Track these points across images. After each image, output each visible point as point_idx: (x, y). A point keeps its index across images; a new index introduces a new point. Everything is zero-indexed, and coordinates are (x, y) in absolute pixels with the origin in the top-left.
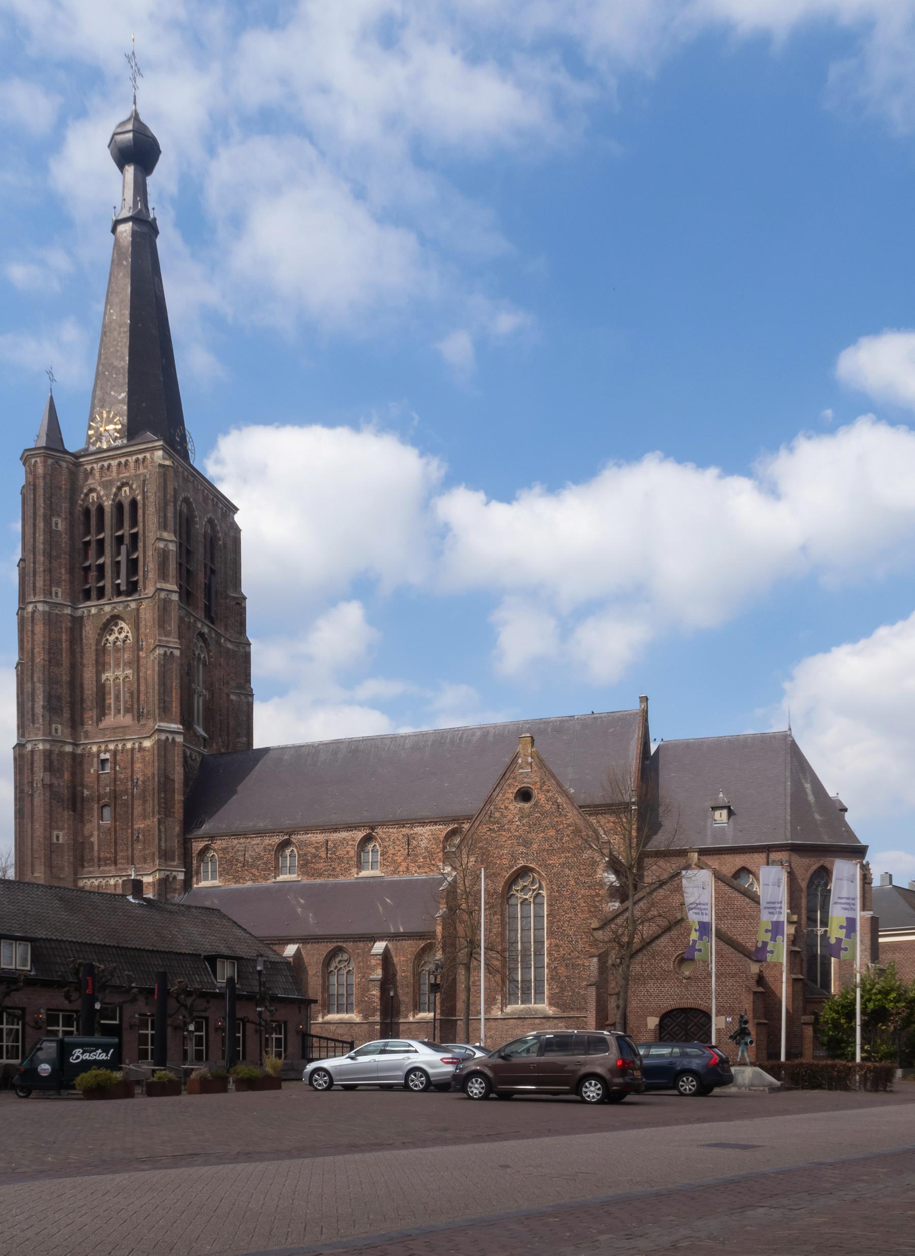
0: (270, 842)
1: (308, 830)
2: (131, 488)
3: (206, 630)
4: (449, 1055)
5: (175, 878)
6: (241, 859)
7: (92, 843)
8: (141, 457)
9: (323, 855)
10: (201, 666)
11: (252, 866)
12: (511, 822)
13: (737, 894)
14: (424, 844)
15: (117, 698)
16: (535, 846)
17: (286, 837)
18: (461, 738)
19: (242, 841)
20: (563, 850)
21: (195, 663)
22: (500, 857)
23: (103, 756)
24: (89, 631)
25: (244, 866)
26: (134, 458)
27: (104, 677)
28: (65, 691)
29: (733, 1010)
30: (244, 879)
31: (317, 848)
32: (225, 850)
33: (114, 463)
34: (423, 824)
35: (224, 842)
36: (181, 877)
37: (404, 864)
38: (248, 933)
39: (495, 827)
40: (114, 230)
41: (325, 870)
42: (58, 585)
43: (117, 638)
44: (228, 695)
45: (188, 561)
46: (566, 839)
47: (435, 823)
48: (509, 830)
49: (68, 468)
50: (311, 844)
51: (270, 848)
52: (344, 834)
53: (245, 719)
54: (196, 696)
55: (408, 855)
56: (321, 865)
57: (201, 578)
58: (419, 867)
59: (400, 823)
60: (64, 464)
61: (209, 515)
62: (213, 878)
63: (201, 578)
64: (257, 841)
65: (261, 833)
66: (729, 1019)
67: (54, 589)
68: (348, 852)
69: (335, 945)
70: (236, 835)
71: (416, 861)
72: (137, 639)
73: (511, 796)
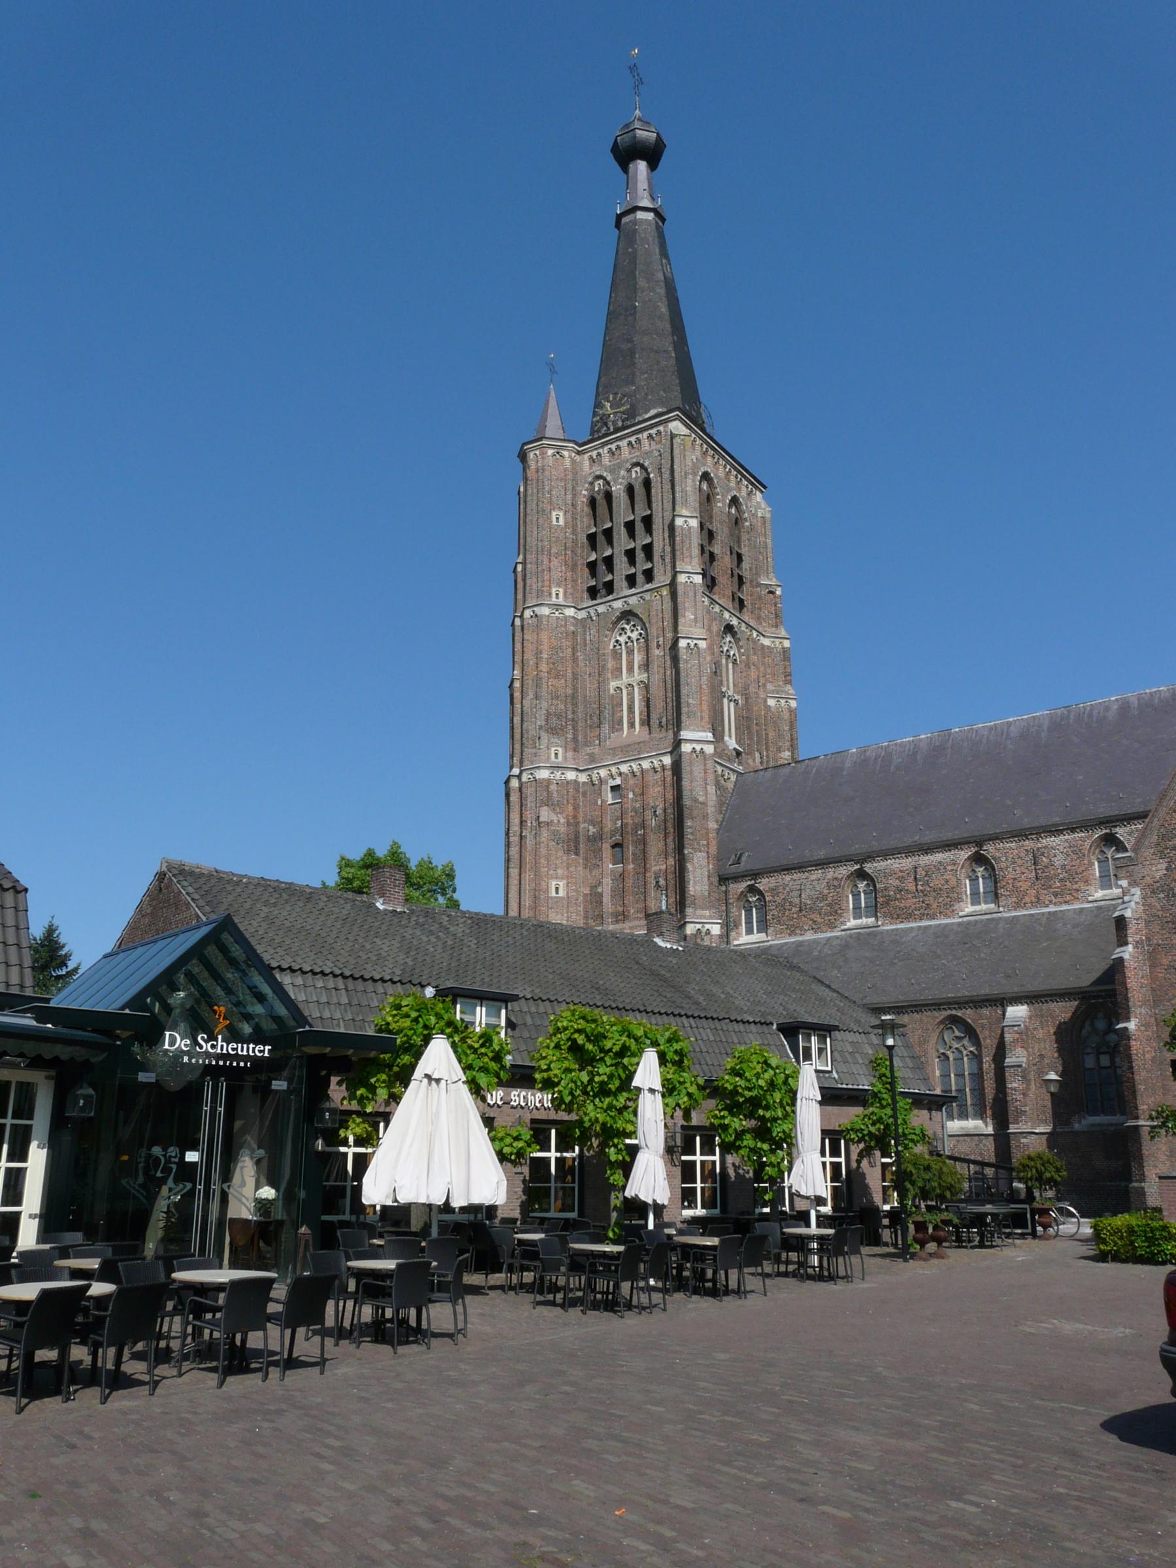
0: (836, 875)
1: (886, 854)
3: (735, 622)
4: (628, 1141)
5: (708, 932)
6: (797, 901)
8: (653, 431)
10: (730, 665)
14: (1059, 861)
17: (857, 867)
18: (1090, 715)
19: (795, 876)
21: (724, 661)
25: (801, 910)
26: (645, 434)
30: (802, 929)
31: (901, 879)
33: (623, 443)
34: (1054, 831)
35: (772, 880)
38: (834, 991)
40: (618, 225)
41: (916, 909)
43: (629, 638)
44: (766, 702)
45: (710, 542)
47: (1073, 830)
49: (570, 457)
50: (893, 873)
51: (835, 883)
52: (940, 856)
53: (787, 728)
54: (725, 701)
55: (1037, 878)
57: (725, 561)
58: (1056, 895)
59: (1021, 834)
60: (566, 453)
61: (734, 493)
64: (817, 874)
65: (822, 864)
67: (554, 590)
68: (947, 881)
69: (949, 1012)
70: (788, 869)
71: (1050, 887)
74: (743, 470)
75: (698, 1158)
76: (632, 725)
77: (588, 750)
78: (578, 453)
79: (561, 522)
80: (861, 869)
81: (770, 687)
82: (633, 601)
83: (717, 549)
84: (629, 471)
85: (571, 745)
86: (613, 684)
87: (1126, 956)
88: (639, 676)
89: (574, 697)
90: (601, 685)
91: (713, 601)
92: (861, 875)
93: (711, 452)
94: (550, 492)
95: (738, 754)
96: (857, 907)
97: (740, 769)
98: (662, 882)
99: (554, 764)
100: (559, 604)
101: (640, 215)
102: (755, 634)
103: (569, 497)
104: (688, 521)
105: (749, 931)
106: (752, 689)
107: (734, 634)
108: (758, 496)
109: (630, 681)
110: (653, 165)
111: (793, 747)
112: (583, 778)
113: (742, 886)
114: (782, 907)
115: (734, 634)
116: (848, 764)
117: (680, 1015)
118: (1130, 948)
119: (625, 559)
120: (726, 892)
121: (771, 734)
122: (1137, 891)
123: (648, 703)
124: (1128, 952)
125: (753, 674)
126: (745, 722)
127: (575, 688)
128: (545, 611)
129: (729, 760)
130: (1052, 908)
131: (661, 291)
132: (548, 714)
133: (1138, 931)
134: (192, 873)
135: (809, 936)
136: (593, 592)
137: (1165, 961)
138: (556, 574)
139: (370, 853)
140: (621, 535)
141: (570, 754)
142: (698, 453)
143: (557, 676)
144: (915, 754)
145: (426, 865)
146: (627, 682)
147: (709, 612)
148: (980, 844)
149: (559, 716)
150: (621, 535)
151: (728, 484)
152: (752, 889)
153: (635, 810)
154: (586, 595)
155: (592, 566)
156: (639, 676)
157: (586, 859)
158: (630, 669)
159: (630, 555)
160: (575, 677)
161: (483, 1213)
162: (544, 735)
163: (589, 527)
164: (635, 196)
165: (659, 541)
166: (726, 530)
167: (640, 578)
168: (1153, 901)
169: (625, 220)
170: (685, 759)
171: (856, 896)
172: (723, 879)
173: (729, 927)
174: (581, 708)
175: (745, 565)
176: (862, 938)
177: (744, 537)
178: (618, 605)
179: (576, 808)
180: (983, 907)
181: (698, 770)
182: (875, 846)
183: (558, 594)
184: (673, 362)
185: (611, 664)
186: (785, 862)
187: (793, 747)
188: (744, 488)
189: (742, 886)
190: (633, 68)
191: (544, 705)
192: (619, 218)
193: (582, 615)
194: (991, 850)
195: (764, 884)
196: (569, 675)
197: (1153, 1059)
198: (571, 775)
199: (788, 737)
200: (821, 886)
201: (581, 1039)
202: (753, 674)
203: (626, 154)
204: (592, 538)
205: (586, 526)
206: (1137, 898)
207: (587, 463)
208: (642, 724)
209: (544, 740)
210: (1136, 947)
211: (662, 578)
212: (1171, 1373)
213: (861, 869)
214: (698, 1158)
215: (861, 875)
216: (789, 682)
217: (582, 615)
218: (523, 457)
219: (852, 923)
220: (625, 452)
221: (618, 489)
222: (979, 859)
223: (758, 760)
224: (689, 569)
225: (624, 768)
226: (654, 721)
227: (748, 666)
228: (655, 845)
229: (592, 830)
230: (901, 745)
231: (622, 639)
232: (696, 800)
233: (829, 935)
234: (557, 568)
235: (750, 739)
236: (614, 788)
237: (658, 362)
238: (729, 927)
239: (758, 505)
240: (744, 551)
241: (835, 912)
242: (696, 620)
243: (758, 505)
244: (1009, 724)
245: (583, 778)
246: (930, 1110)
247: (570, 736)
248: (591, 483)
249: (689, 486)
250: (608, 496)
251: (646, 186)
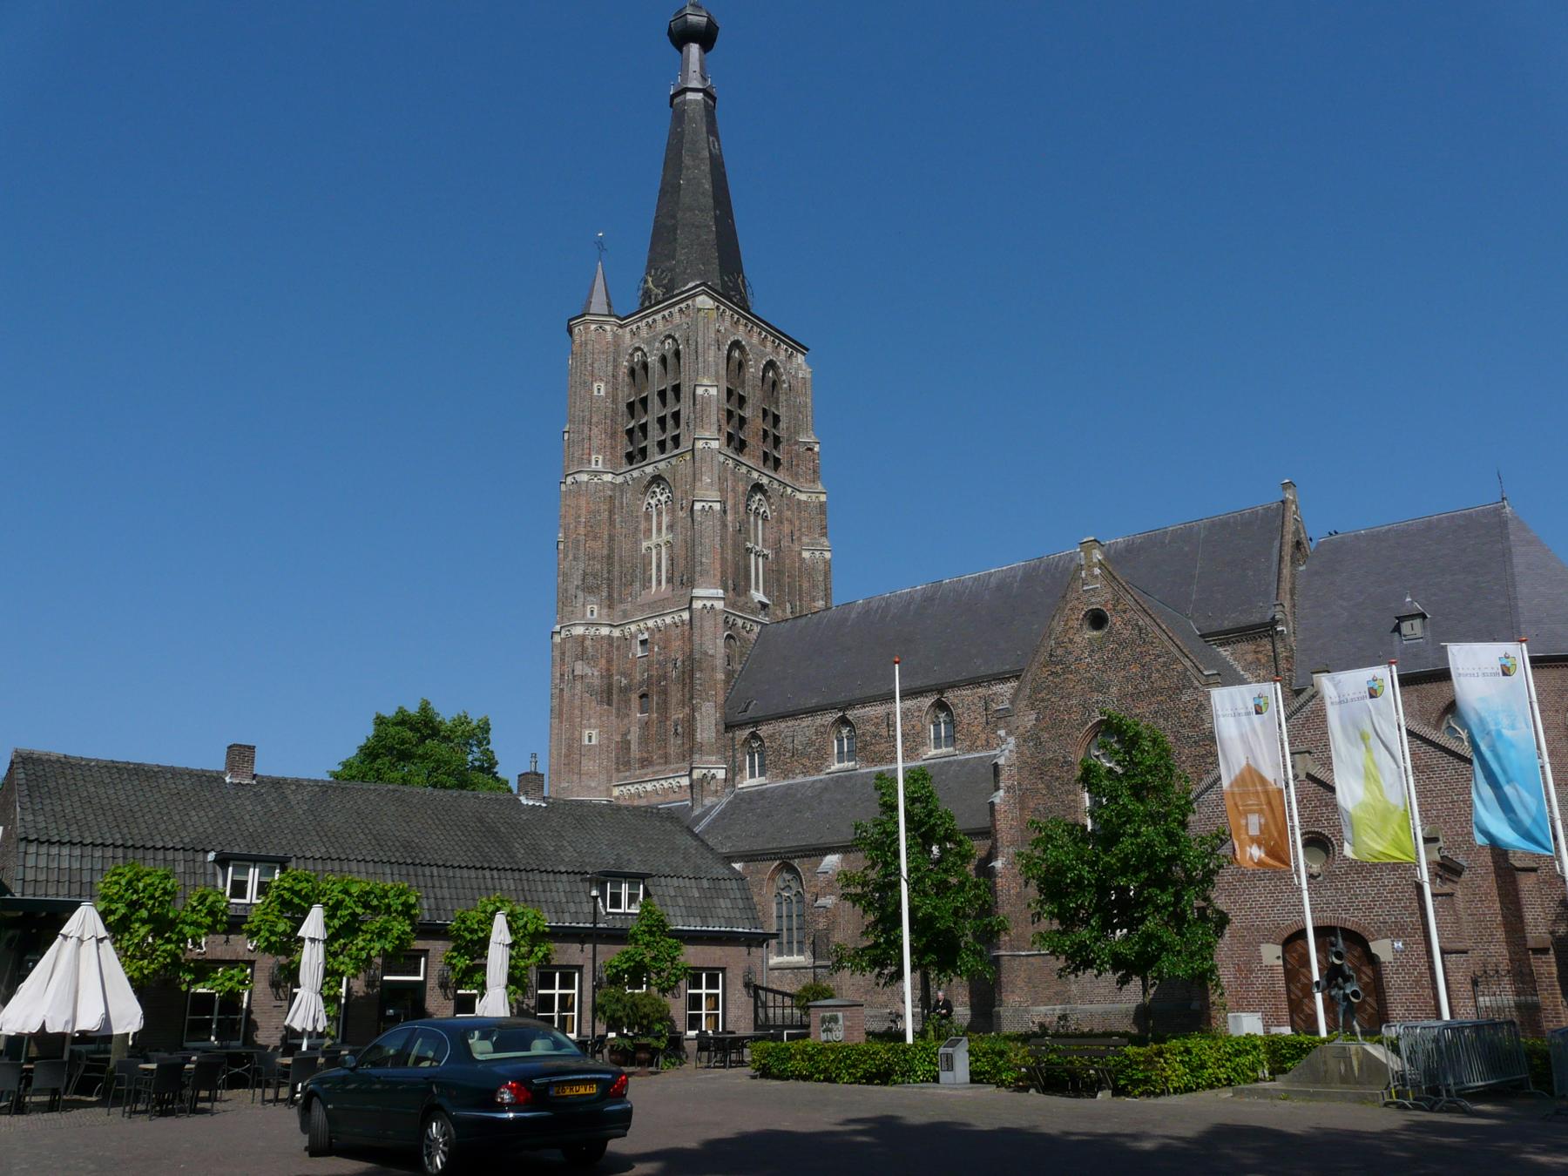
1: (864, 702)
3: (765, 481)
5: (714, 777)
8: (683, 305)
16: (1114, 690)
20: (1154, 692)
22: (1069, 710)
29: (1403, 929)
30: (793, 771)
33: (658, 317)
36: (721, 774)
37: (983, 736)
46: (1155, 675)
48: (1077, 671)
57: (756, 423)
59: (975, 682)
60: (608, 328)
63: (756, 423)
64: (807, 721)
65: (811, 712)
66: (1399, 945)
74: (780, 335)
75: (704, 991)
76: (659, 582)
77: (623, 607)
78: (621, 326)
79: (602, 393)
80: (843, 717)
81: (805, 540)
82: (662, 465)
83: (747, 413)
84: (663, 342)
85: (606, 602)
86: (645, 544)
87: (997, 801)
88: (666, 536)
89: (610, 557)
90: (637, 543)
91: (738, 463)
92: (844, 721)
93: (743, 321)
94: (592, 365)
95: (764, 606)
96: (840, 752)
97: (766, 620)
98: (680, 730)
99: (591, 621)
100: (599, 470)
101: (690, 96)
102: (789, 490)
103: (610, 368)
104: (710, 390)
105: (752, 775)
106: (784, 543)
107: (764, 492)
108: (800, 358)
109: (659, 541)
111: (827, 597)
112: (617, 633)
113: (747, 732)
114: (778, 753)
115: (764, 492)
117: (483, 868)
118: (1001, 793)
119: (657, 426)
120: (733, 739)
121: (805, 585)
122: (1012, 740)
123: (671, 559)
124: (999, 797)
125: (786, 528)
126: (776, 577)
127: (611, 549)
128: (584, 477)
129: (753, 612)
131: (706, 168)
132: (585, 574)
133: (1011, 777)
134: (39, 759)
135: (800, 779)
136: (630, 458)
137: (1032, 805)
138: (595, 443)
139: (401, 711)
140: (655, 402)
141: (605, 611)
142: (727, 323)
143: (595, 538)
145: (463, 721)
146: (656, 542)
147: (734, 473)
148: (941, 692)
149: (595, 576)
150: (655, 402)
151: (759, 348)
152: (754, 736)
153: (659, 662)
154: (624, 461)
155: (630, 432)
156: (666, 536)
157: (618, 709)
158: (659, 530)
159: (662, 421)
160: (611, 538)
161: (100, 1040)
162: (580, 594)
163: (629, 396)
164: (685, 79)
165: (685, 407)
166: (759, 394)
167: (669, 444)
169: (677, 100)
170: (697, 615)
171: (840, 741)
172: (729, 727)
173: (734, 771)
174: (617, 567)
175: (782, 425)
176: (841, 781)
177: (782, 398)
178: (649, 469)
179: (609, 661)
180: (944, 750)
181: (708, 625)
182: (858, 694)
183: (598, 461)
184: (713, 236)
185: (642, 526)
186: (781, 710)
187: (827, 597)
188: (782, 353)
189: (747, 732)
191: (582, 566)
192: (673, 97)
193: (620, 480)
194: (950, 697)
195: (764, 731)
196: (606, 537)
197: (1018, 895)
198: (605, 631)
199: (822, 587)
200: (810, 733)
201: (287, 895)
202: (786, 528)
203: (681, 37)
204: (631, 406)
205: (626, 394)
206: (1011, 747)
207: (628, 336)
209: (581, 600)
210: (1007, 791)
211: (685, 445)
213: (843, 717)
214: (704, 991)
215: (844, 721)
216: (824, 535)
217: (620, 480)
218: (570, 331)
219: (836, 766)
220: (660, 326)
221: (653, 360)
222: (941, 706)
223: (789, 610)
224: (707, 435)
225: (650, 623)
226: (677, 580)
227: (780, 521)
228: (675, 695)
229: (624, 682)
230: (900, 596)
231: (653, 502)
232: (706, 653)
233: (816, 778)
234: (598, 436)
235: (781, 589)
236: (643, 642)
237: (699, 237)
238: (734, 771)
239: (799, 367)
240: (782, 412)
241: (822, 756)
242: (712, 484)
243: (799, 367)
244: (990, 575)
245: (617, 633)
246: (749, 946)
247: (605, 594)
248: (632, 355)
249: (714, 358)
250: (645, 366)
251: (697, 68)
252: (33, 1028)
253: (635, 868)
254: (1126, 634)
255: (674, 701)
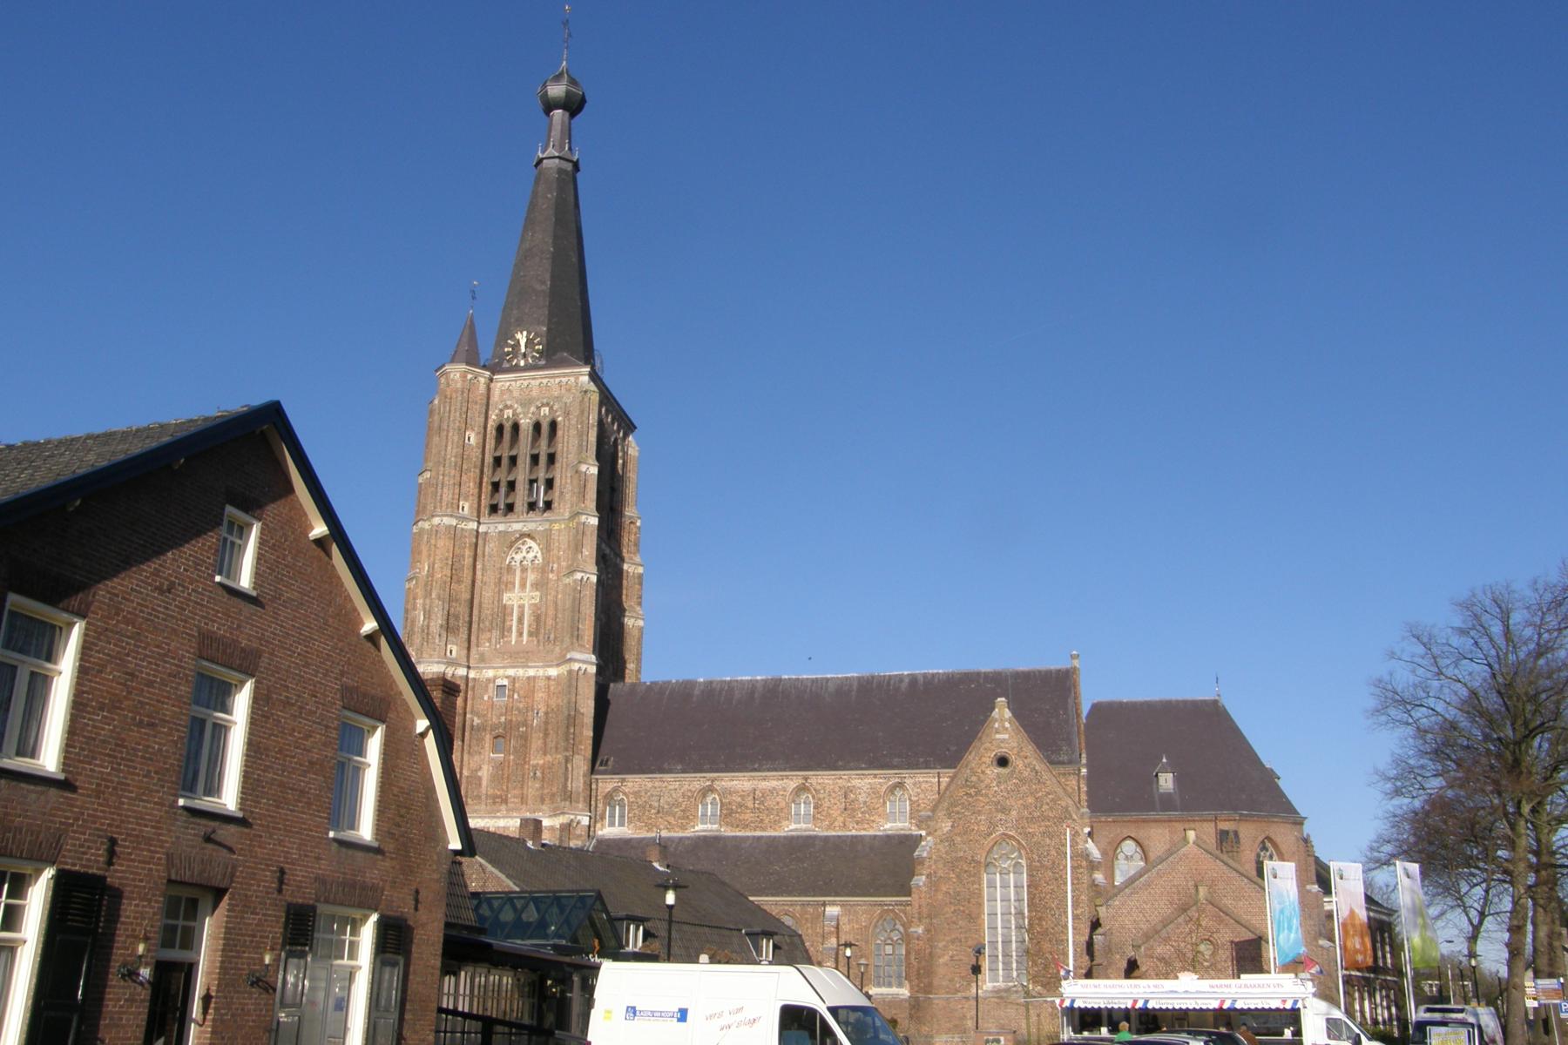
2: (551, 408)
7: (480, 779)
9: (750, 805)
11: (669, 813)
12: (988, 787)
13: (1234, 874)
15: (520, 620)
16: (1014, 813)
23: (499, 682)
24: (491, 547)
27: (506, 596)
28: (462, 610)
32: (637, 794)
36: (585, 821)
39: (972, 791)
42: (466, 499)
56: (748, 816)
62: (621, 824)
72: (546, 562)
73: (988, 761)
76: (520, 634)
98: (539, 774)
105: (612, 824)
110: (573, 114)
116: (697, 692)
130: (854, 833)
144: (753, 692)
158: (523, 586)
168: (940, 847)
190: (566, 23)
208: (530, 634)
212: (1282, 795)
221: (526, 423)
244: (828, 680)
252: (1214, 1005)
253: (639, 913)
254: (1026, 774)
255: (534, 746)
